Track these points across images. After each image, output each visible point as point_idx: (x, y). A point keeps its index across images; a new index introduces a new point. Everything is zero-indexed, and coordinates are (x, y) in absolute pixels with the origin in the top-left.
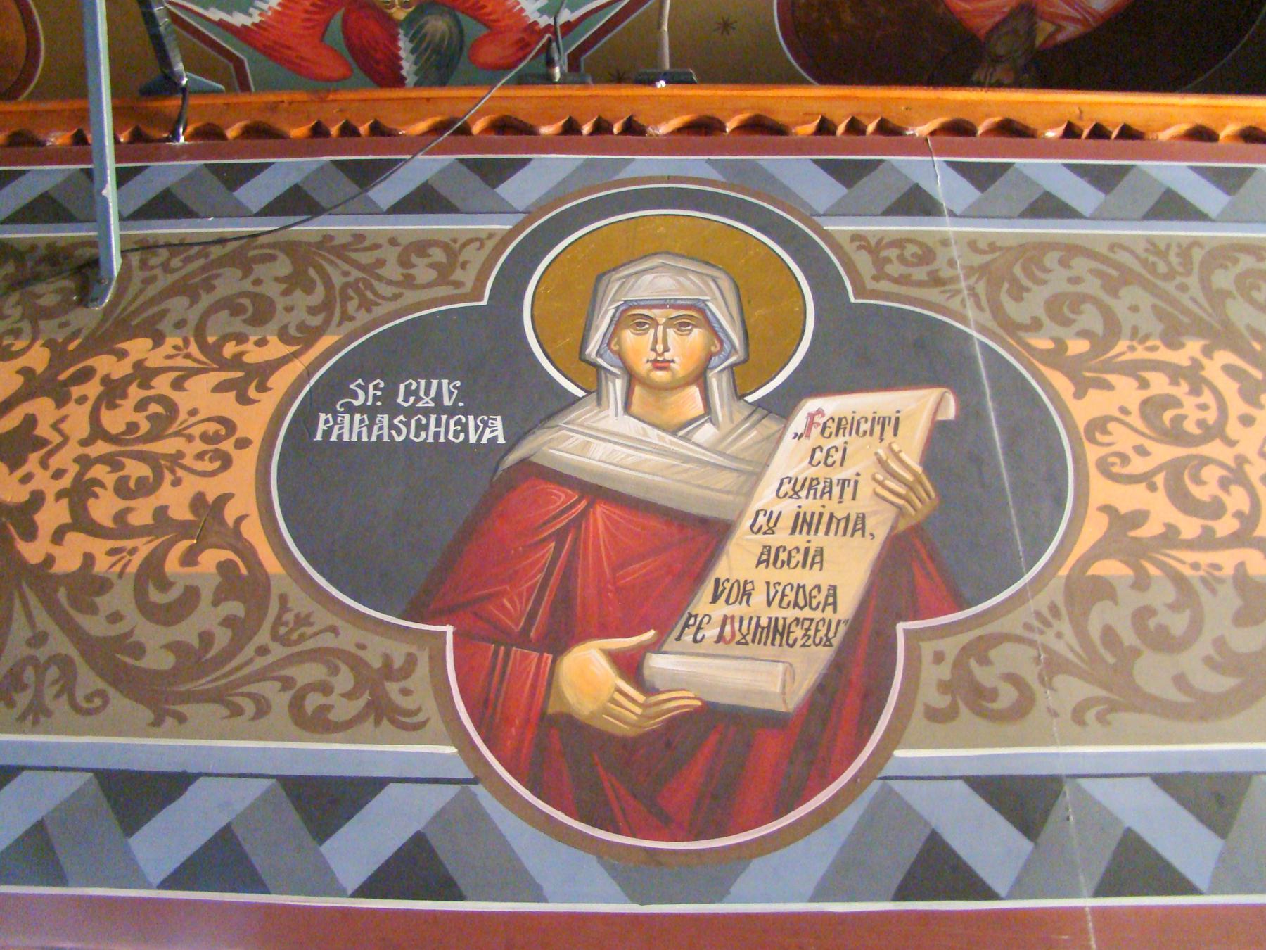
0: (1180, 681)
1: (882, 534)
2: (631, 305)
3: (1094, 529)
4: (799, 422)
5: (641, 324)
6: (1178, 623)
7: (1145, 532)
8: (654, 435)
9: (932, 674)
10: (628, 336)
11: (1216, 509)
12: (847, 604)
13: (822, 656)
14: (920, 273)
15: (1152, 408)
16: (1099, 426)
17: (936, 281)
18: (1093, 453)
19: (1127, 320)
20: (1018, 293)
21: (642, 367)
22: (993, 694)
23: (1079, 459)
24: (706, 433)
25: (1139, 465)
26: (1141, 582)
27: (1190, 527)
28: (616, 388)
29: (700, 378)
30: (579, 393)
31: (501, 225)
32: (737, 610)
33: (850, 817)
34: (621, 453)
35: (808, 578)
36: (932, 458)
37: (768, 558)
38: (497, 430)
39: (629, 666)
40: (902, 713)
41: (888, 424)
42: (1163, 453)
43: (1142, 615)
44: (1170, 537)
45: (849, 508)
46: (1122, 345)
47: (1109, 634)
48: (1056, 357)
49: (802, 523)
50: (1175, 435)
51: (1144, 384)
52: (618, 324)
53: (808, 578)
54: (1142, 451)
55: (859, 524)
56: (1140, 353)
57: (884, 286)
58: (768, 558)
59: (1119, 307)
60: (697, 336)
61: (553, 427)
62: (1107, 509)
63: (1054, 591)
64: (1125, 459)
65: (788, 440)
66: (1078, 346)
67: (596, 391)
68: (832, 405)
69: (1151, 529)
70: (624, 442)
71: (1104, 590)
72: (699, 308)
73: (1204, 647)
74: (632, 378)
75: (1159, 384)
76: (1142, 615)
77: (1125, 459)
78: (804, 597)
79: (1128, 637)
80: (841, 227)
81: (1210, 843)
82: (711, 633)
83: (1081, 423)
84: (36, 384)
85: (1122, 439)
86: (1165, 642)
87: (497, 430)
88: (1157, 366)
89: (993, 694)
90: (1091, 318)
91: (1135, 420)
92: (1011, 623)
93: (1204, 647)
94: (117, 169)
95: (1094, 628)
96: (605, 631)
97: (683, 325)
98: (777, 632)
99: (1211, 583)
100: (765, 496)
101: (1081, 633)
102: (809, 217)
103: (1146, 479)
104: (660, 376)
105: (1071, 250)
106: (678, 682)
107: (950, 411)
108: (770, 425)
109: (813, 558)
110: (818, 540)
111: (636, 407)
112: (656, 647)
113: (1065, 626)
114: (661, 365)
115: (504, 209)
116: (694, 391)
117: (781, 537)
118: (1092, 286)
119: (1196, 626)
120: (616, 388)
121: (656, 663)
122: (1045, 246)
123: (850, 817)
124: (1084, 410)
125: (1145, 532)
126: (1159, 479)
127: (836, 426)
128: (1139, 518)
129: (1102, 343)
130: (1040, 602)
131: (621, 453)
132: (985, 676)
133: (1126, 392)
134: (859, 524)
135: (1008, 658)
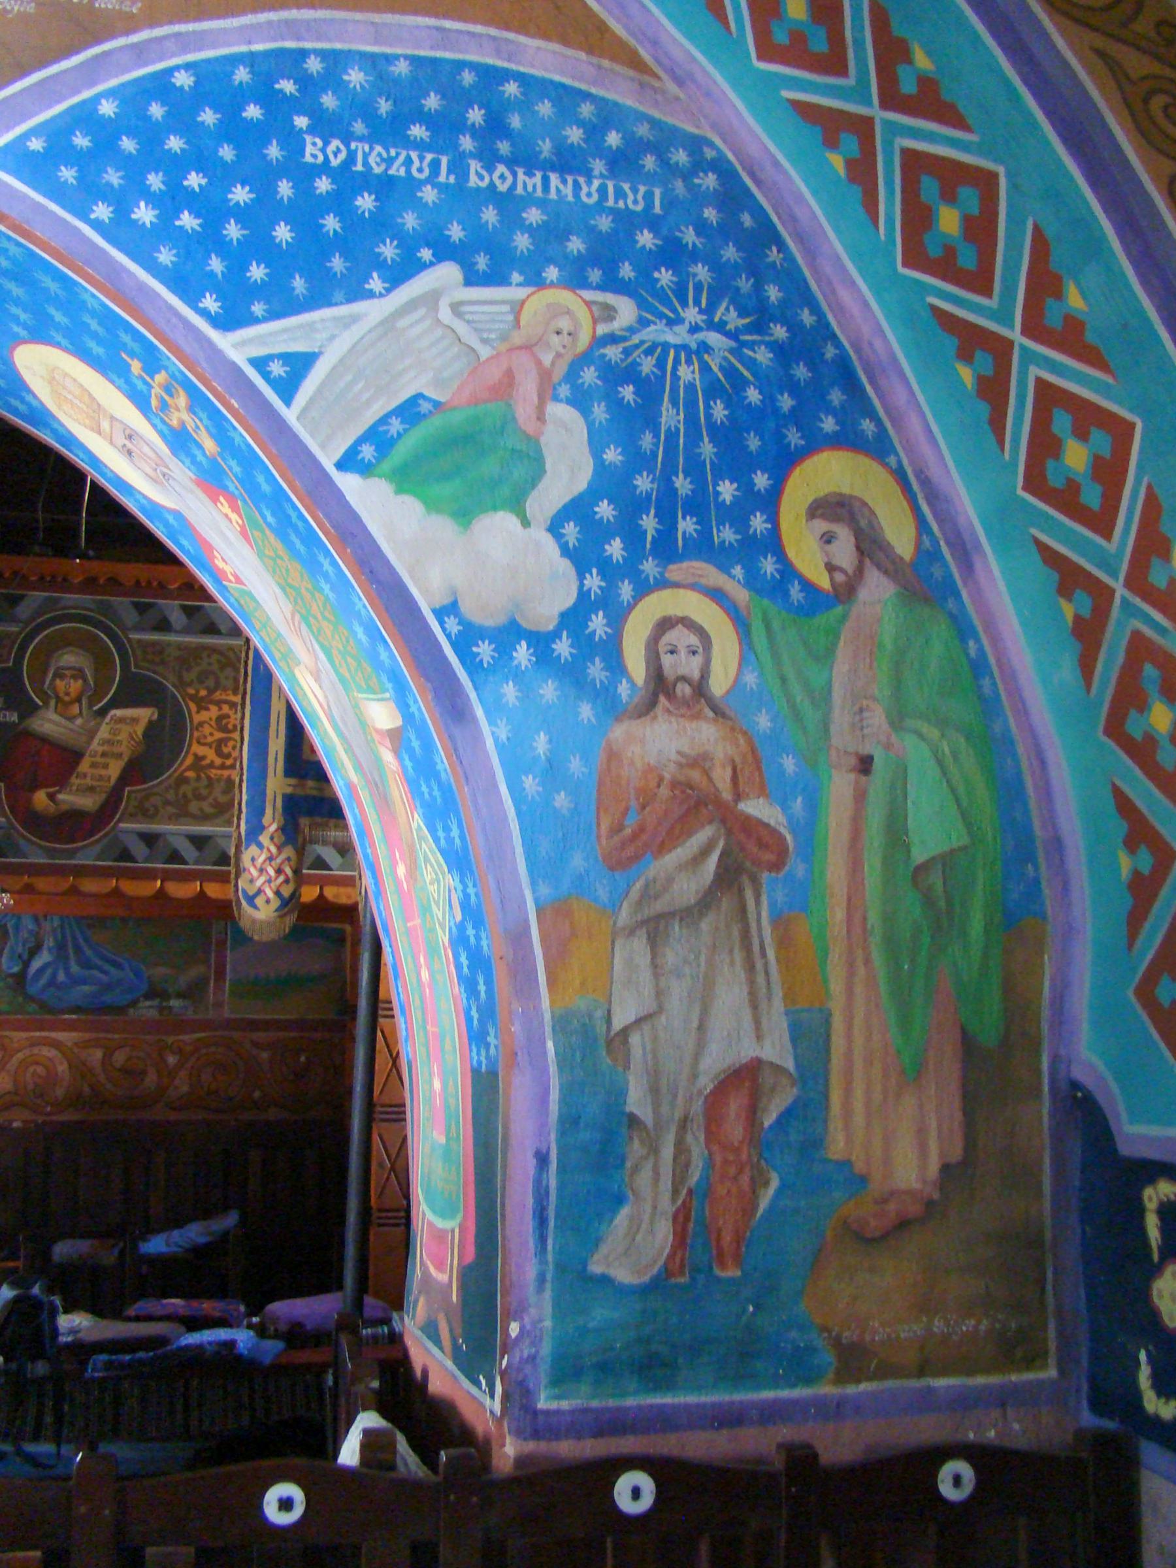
0: (201, 809)
1: (126, 759)
2: (58, 669)
3: (189, 761)
4: (107, 719)
5: (62, 677)
6: (204, 792)
7: (204, 763)
8: (63, 721)
9: (133, 803)
10: (58, 682)
11: (228, 756)
12: (113, 781)
13: (104, 796)
14: (157, 659)
15: (220, 718)
16: (201, 724)
17: (163, 663)
18: (196, 734)
19: (223, 682)
20: (189, 669)
21: (61, 695)
22: (148, 810)
23: (191, 735)
24: (79, 721)
25: (210, 739)
26: (198, 778)
27: (218, 761)
28: (53, 703)
29: (78, 700)
30: (40, 703)
31: (15, 629)
32: (83, 782)
33: (105, 841)
34: (55, 728)
35: (103, 772)
36: (146, 735)
37: (94, 765)
38: (14, 718)
39: (51, 797)
40: (123, 814)
41: (135, 721)
42: (219, 735)
43: (195, 790)
44: (212, 765)
45: (116, 750)
46: (218, 693)
47: (185, 796)
48: (193, 698)
49: (104, 755)
50: (224, 729)
51: (220, 709)
52: (56, 675)
53: (103, 772)
54: (211, 734)
55: (119, 756)
56: (224, 697)
57: (146, 665)
58: (94, 765)
59: (222, 676)
60: (80, 682)
61: (376, 327)
62: (195, 755)
63: (171, 781)
64: (205, 737)
65: (104, 725)
66: (203, 693)
67: (46, 704)
68: (118, 713)
69: (207, 761)
70: (856, 1031)
71: (186, 780)
72: (81, 670)
73: (210, 800)
74: (58, 698)
75: (226, 709)
76: (195, 790)
77: (205, 737)
78: (101, 778)
79: (190, 795)
80: (135, 636)
81: (196, 854)
82: (74, 788)
83: (196, 721)
84: (704, 811)
85: (207, 730)
86: (199, 797)
87: (14, 718)
88: (226, 702)
89: (148, 810)
90: (211, 682)
91: (213, 723)
92: (156, 790)
93: (210, 800)
94: (229, 865)
95: (181, 792)
96: (47, 786)
97: (75, 677)
98: (91, 789)
99: (219, 780)
100: (95, 745)
101: (177, 795)
102: (125, 629)
103: (210, 745)
104: (67, 699)
105: (213, 650)
106: (64, 801)
107: (156, 716)
108: (98, 719)
109: (106, 766)
110: (108, 760)
111: (59, 709)
112: (59, 792)
113: (172, 791)
114: (67, 694)
115: (14, 620)
116: (77, 705)
117: (99, 759)
118: (216, 667)
119: (210, 793)
120: (53, 703)
121: (60, 797)
122: (204, 647)
123: (105, 841)
124: (197, 718)
125: (204, 763)
126: (214, 745)
127: (121, 720)
128: (203, 758)
129: (211, 692)
130: (166, 784)
131: (55, 728)
132: (147, 805)
133: (214, 712)
134: (119, 756)
135: (154, 800)
